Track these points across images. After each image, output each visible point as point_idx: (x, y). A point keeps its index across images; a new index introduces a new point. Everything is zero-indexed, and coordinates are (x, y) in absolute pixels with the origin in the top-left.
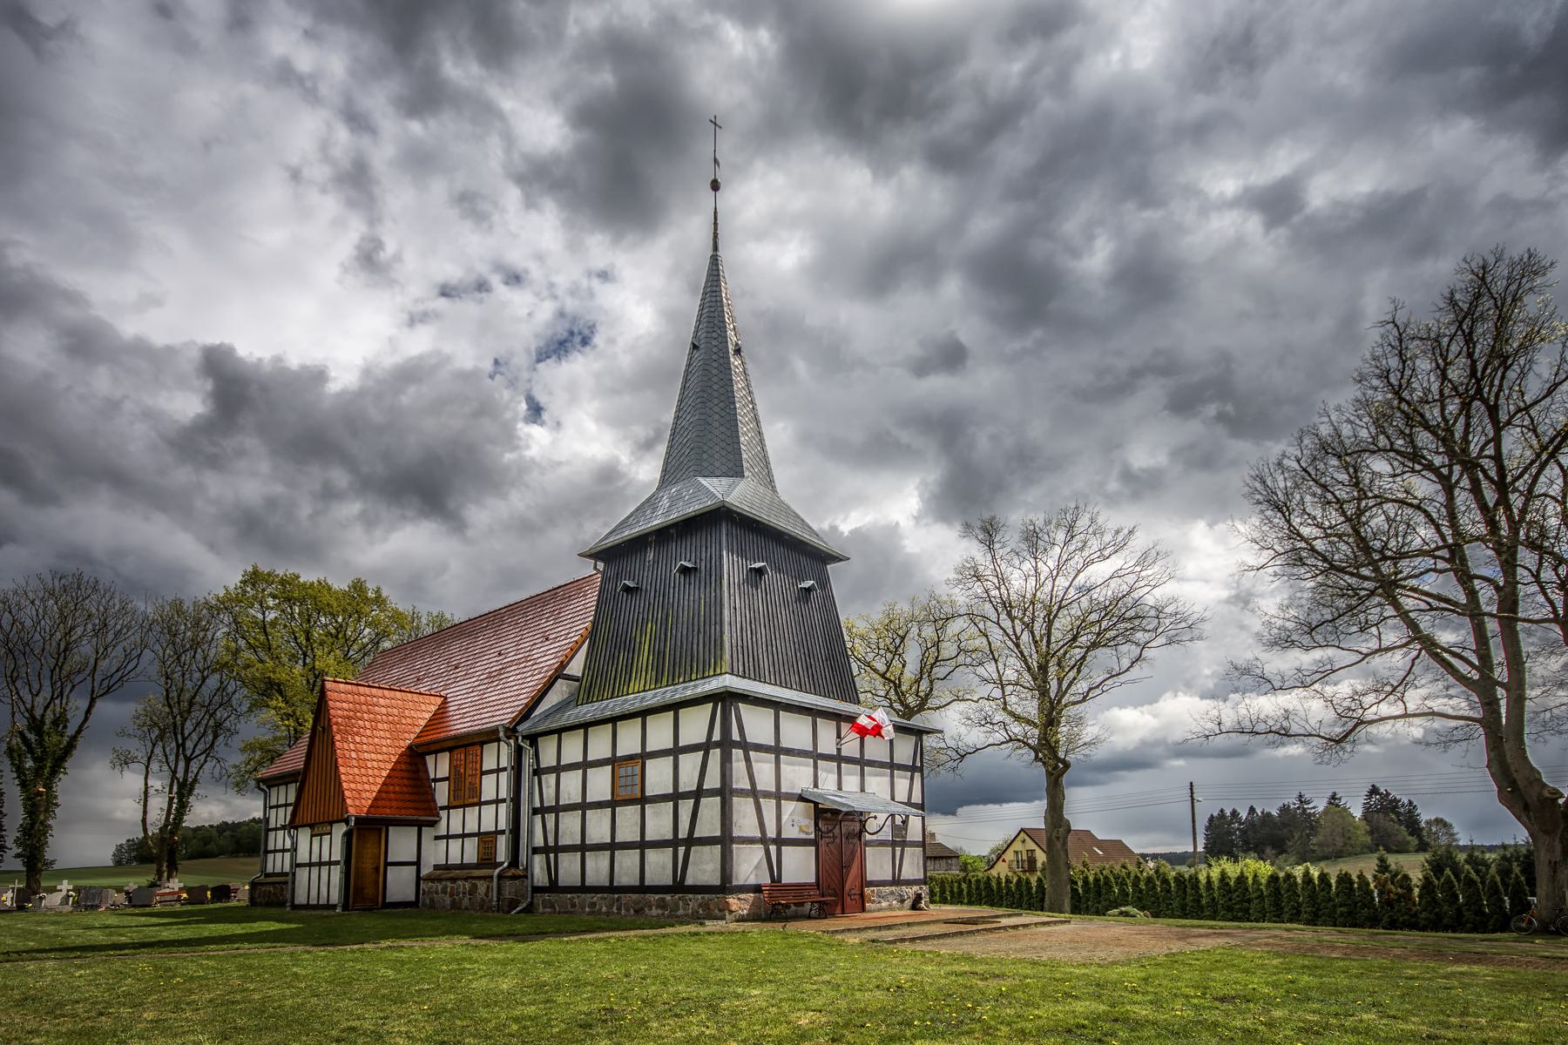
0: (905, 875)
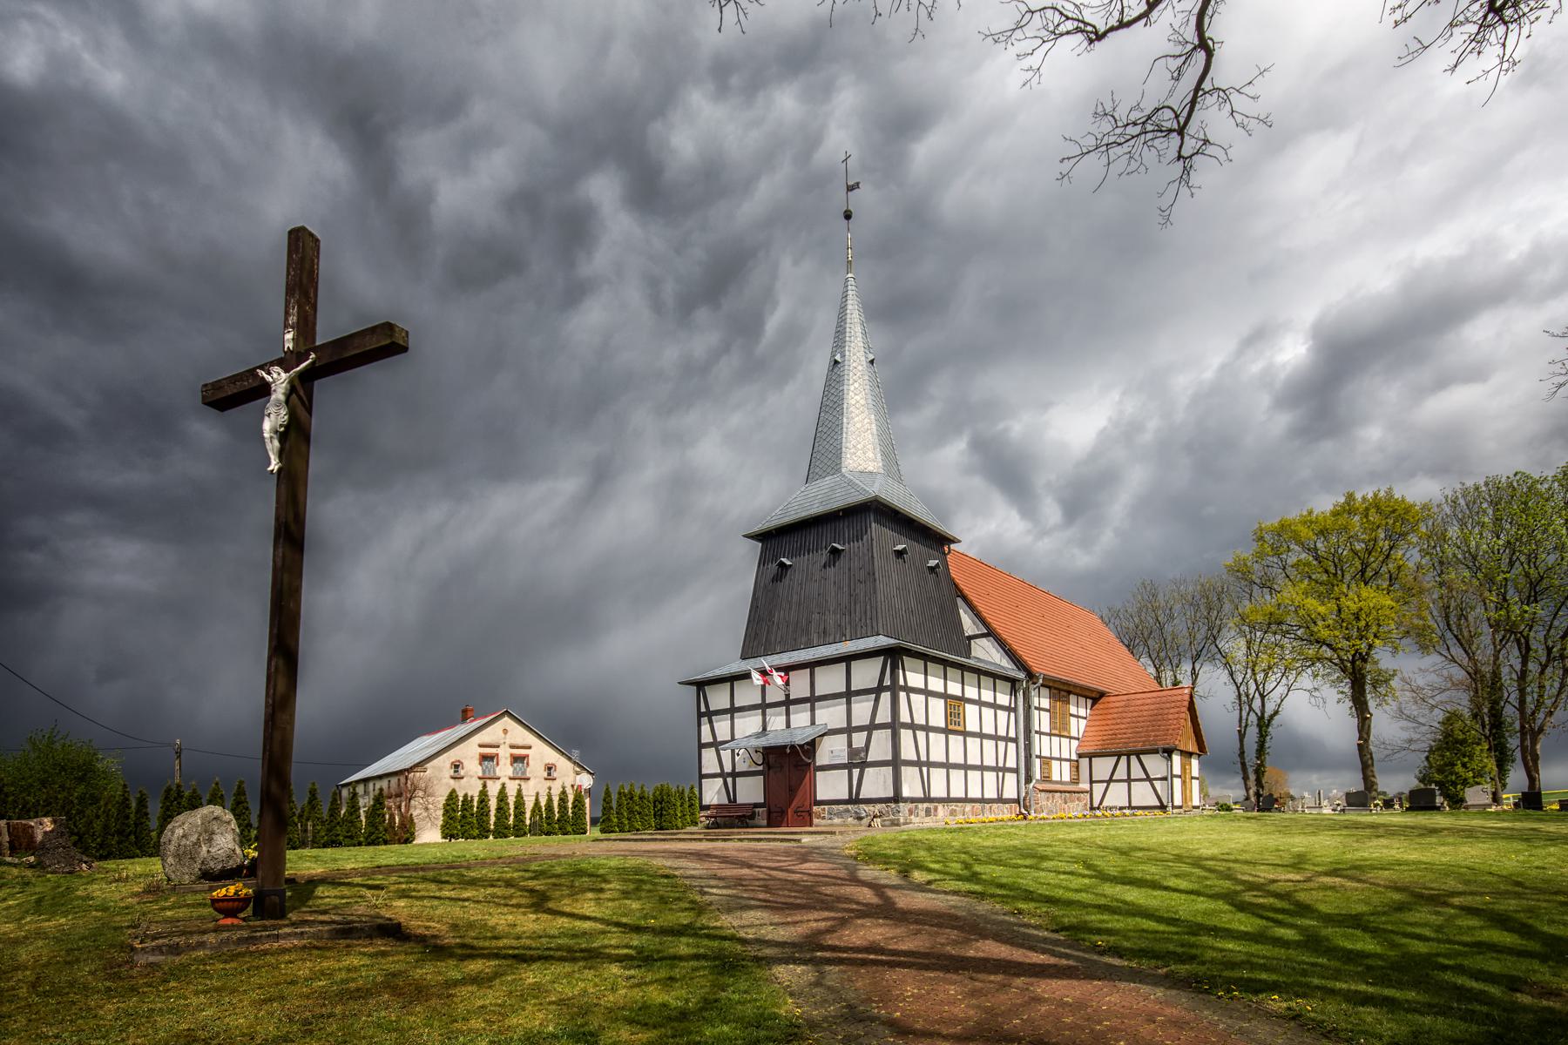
0: (1006, 795)
